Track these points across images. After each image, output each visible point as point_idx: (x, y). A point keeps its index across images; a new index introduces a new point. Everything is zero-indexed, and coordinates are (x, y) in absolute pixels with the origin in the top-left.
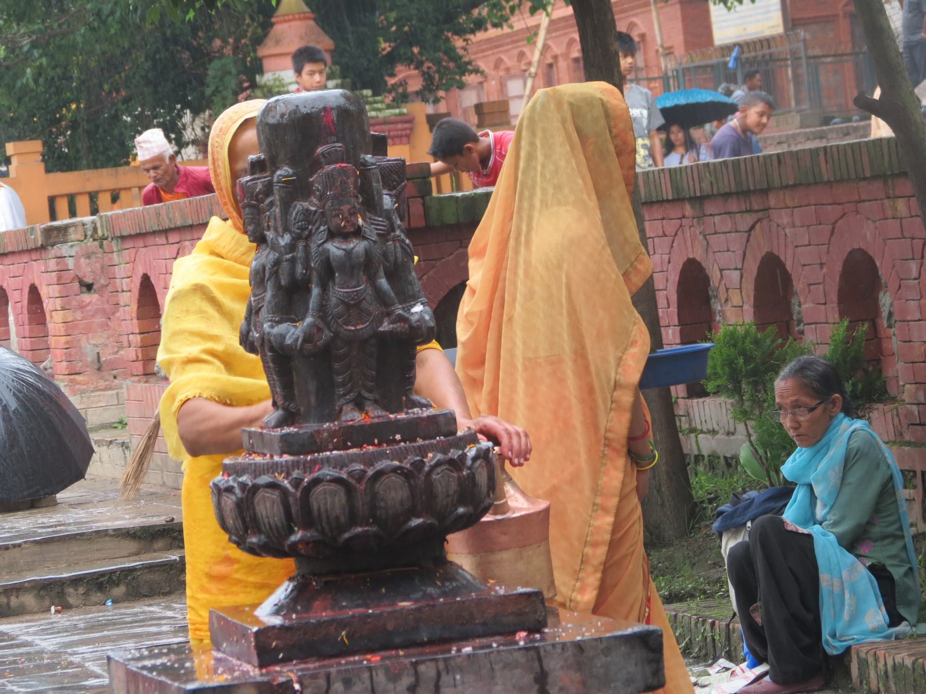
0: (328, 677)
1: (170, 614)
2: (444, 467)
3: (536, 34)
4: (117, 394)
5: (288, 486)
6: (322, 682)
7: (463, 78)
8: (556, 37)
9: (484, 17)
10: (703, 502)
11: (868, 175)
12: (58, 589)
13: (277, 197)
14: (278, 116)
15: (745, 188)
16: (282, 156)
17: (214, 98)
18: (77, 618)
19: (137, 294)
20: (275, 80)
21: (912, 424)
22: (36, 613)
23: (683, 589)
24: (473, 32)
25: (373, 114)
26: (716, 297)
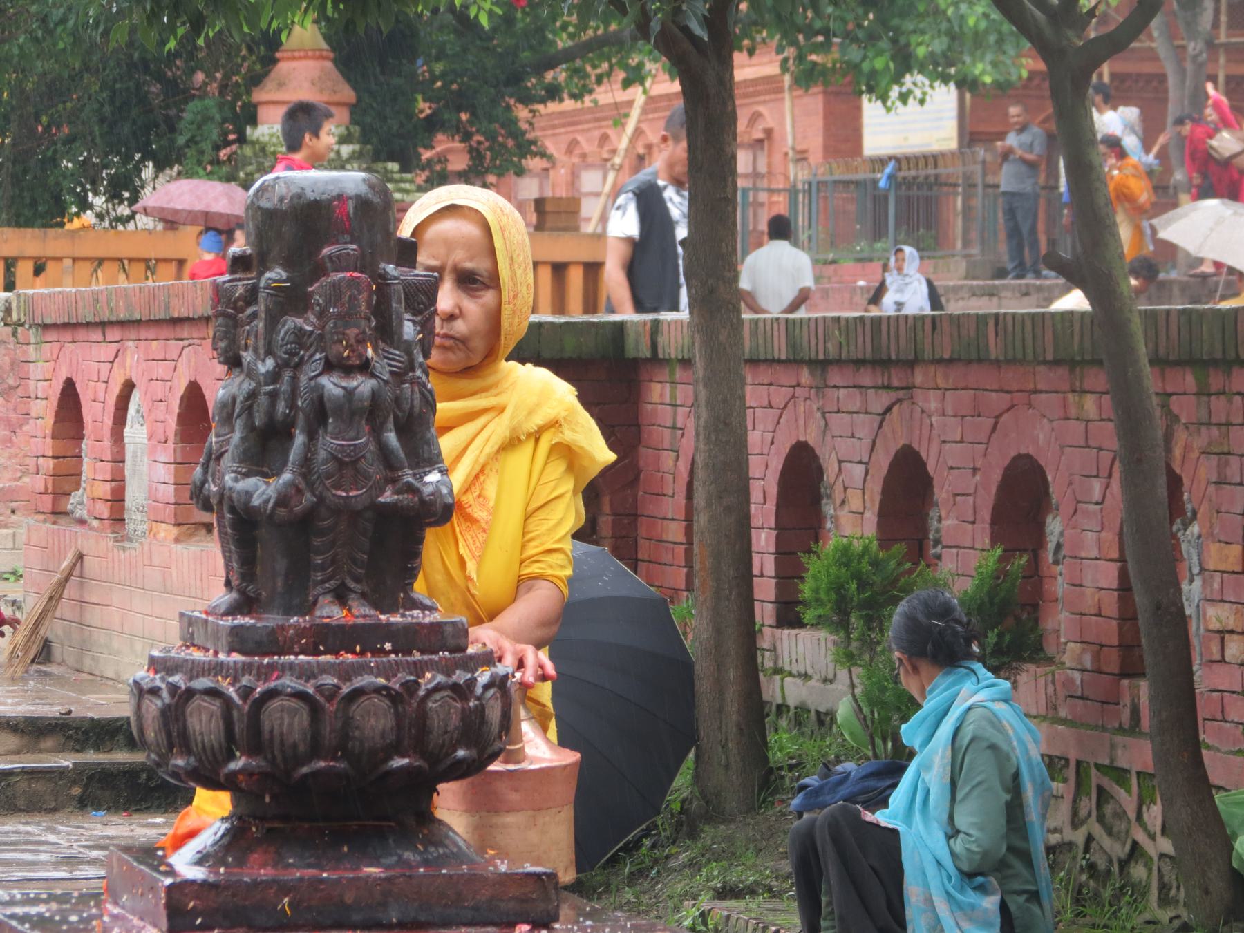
1: (52, 838)
2: (445, 693)
3: (627, 116)
4: (14, 535)
8: (654, 119)
9: (560, 84)
10: (781, 768)
13: (263, 307)
14: (276, 200)
15: (884, 357)
16: (274, 253)
19: (55, 404)
21: (1071, 696)
23: (742, 882)
24: (543, 101)
26: (829, 497)
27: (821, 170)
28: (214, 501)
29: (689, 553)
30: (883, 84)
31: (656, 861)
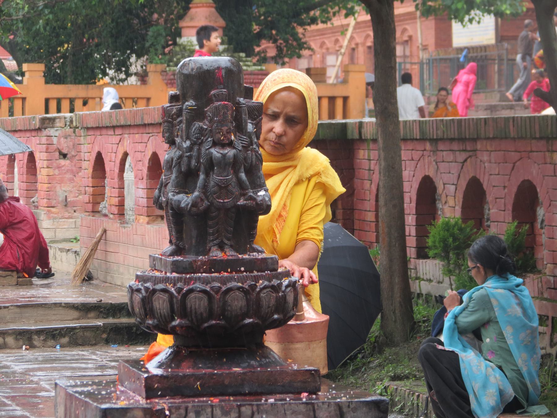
0: (186, 409)
1: (94, 357)
2: (268, 290)
3: (347, 30)
4: (75, 222)
5: (174, 292)
6: (182, 411)
7: (301, 52)
8: (359, 32)
9: (316, 17)
10: (420, 322)
11: (538, 136)
12: (27, 336)
13: (184, 118)
14: (190, 70)
15: (463, 137)
17: (150, 49)
18: (38, 354)
19: (93, 163)
20: (188, 42)
21: (549, 288)
22: (14, 348)
23: (402, 373)
24: (309, 24)
25: (244, 68)
27: (434, 54)
28: (164, 205)
29: (377, 226)
30: (461, 15)
31: (364, 364)
